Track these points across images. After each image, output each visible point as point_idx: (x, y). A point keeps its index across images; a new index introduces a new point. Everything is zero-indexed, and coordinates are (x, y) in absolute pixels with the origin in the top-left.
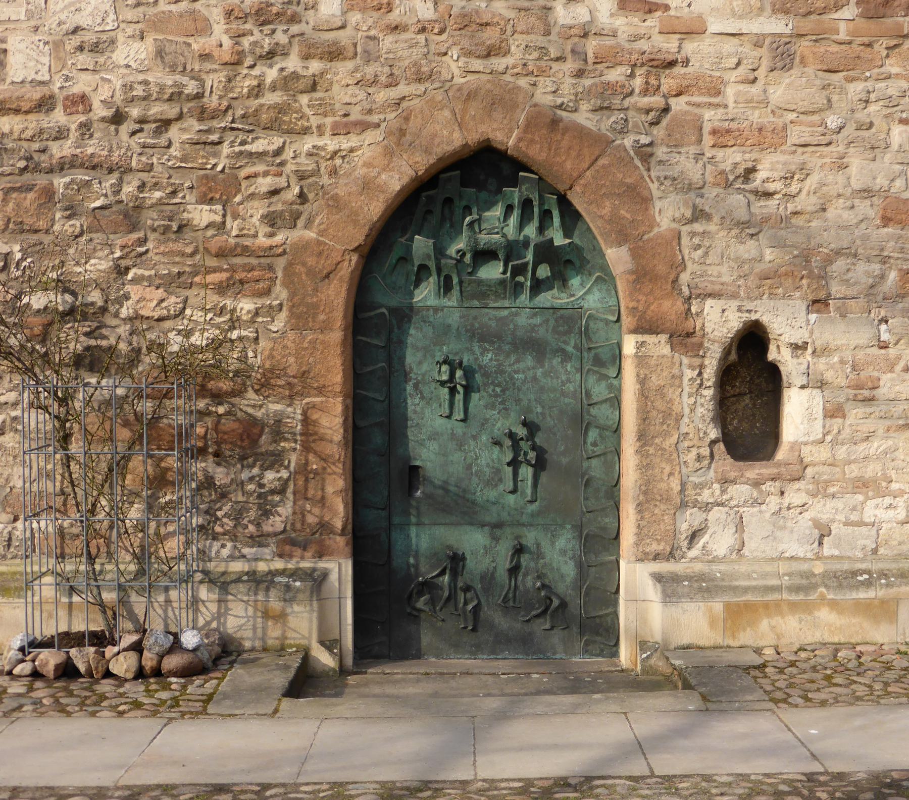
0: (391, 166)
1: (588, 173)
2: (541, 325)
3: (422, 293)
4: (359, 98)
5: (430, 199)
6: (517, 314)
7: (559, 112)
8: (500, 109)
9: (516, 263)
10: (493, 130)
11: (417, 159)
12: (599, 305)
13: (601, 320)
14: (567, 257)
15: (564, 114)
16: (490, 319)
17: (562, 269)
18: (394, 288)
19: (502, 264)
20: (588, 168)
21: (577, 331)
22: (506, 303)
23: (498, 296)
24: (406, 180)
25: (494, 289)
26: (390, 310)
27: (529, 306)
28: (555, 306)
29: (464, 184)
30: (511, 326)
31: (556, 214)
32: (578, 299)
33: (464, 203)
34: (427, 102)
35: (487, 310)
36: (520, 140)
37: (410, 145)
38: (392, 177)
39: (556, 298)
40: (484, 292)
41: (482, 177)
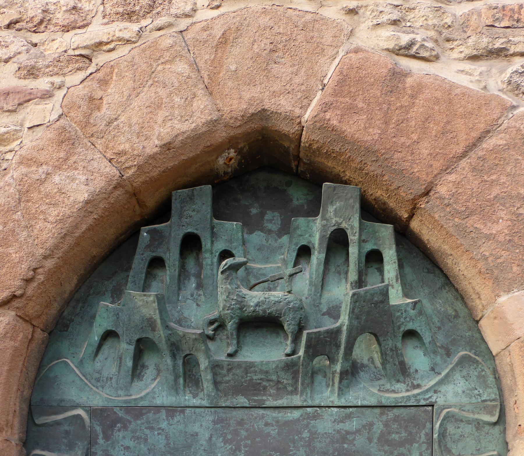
0: (71, 162)
1: (464, 163)
2: (358, 431)
3: (147, 386)
4: (13, 49)
5: (157, 238)
6: (315, 417)
7: (405, 63)
8: (286, 60)
9: (310, 331)
10: (274, 94)
11: (121, 148)
12: (465, 400)
13: (469, 422)
14: (410, 326)
15: (414, 65)
16: (267, 424)
17: (399, 345)
18: (98, 380)
19: (289, 342)
20: (464, 155)
21: (423, 438)
22: (297, 400)
23: (281, 389)
24: (99, 183)
25: (274, 378)
26: (93, 412)
27: (337, 403)
28: (384, 402)
29: (219, 213)
30: (306, 434)
31: (390, 255)
32: (427, 391)
33: (220, 246)
34: (144, 51)
35: (261, 412)
36: (326, 107)
37: (109, 123)
38: (73, 180)
39: (387, 391)
40: (252, 385)
41: (254, 211)
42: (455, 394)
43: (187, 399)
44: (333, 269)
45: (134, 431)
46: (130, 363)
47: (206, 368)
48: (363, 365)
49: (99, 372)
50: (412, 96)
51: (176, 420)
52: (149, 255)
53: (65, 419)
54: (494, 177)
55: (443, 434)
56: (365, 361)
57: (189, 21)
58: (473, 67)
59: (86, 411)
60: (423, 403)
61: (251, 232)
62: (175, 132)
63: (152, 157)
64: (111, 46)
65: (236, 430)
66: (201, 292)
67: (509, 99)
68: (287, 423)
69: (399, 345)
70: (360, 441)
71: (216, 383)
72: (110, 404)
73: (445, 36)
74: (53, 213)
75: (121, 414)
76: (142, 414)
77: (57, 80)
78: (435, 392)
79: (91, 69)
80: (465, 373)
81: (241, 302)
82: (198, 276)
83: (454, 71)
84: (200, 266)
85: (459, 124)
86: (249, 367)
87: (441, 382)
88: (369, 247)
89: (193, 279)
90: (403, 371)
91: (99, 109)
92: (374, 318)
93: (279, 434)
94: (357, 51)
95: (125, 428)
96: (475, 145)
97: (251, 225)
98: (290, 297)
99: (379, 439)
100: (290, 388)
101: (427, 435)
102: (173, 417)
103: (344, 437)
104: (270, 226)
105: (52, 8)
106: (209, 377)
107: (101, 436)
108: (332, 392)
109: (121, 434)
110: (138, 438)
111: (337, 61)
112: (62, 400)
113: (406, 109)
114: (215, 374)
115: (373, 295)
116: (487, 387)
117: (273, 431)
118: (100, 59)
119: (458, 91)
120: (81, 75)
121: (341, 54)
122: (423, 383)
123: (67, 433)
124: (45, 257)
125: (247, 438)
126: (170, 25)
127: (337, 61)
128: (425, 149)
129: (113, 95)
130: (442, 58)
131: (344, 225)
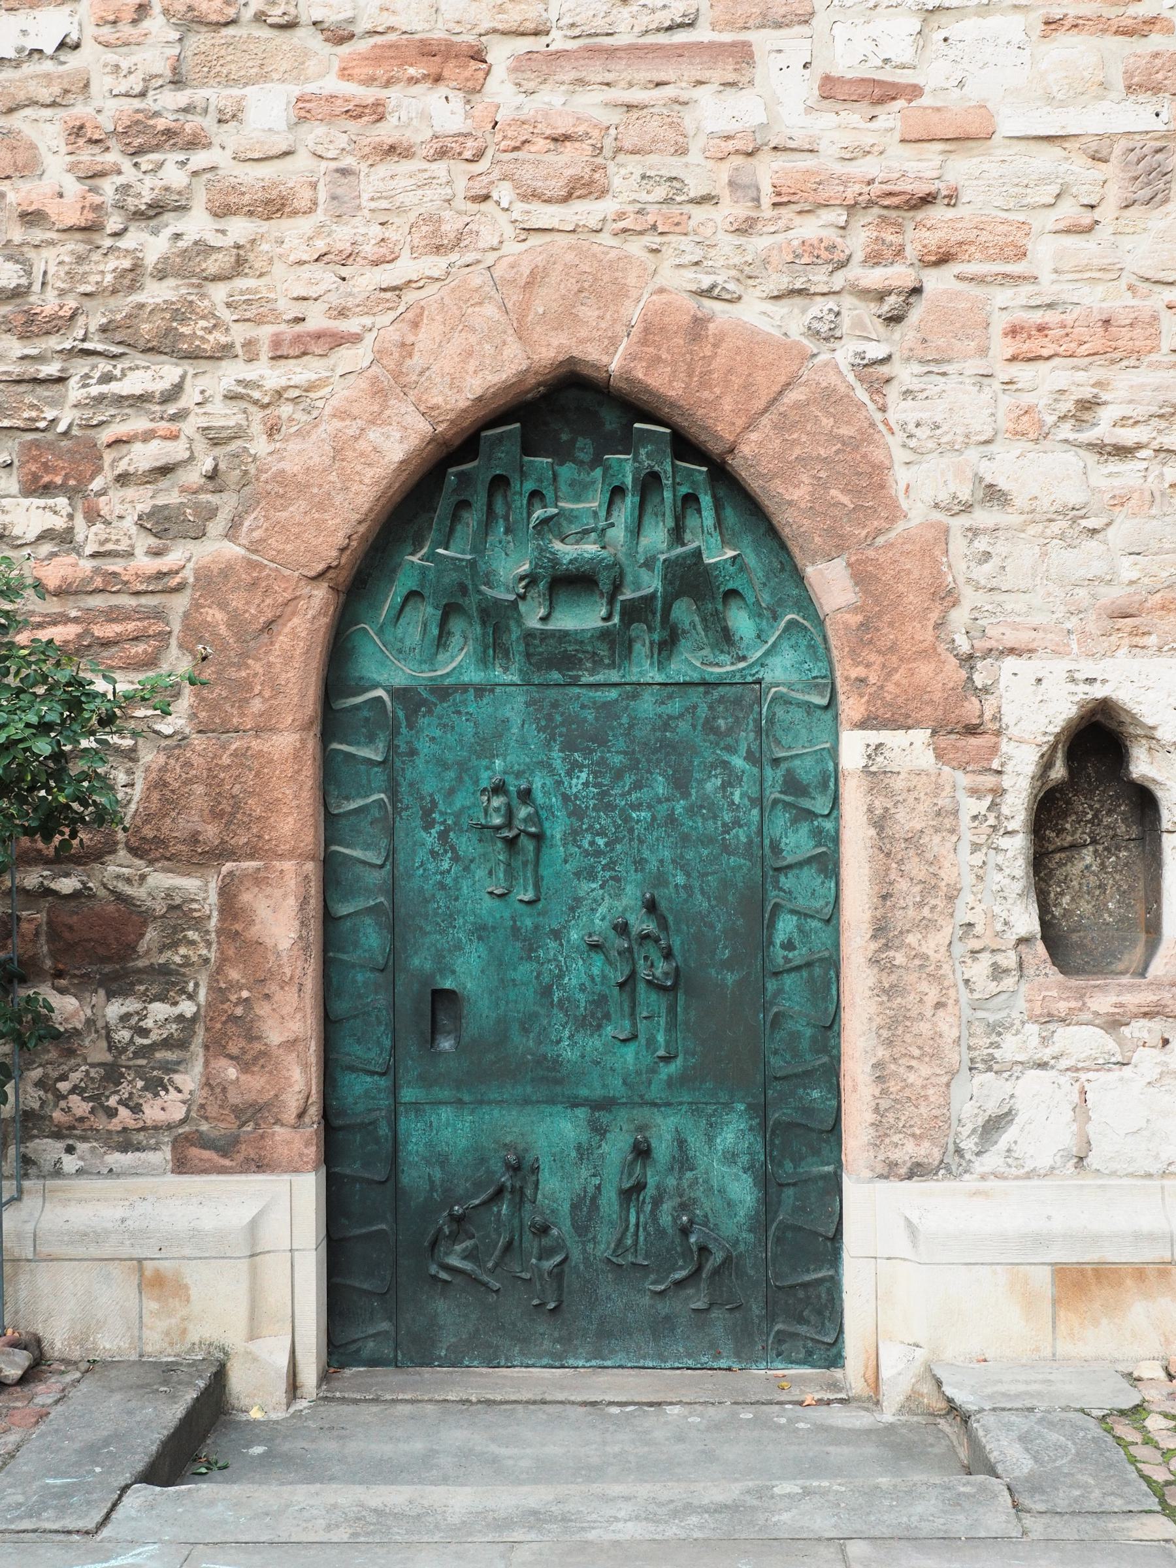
0: (384, 416)
1: (765, 420)
2: (681, 715)
3: (453, 658)
8: (592, 301)
10: (581, 342)
11: (434, 401)
12: (795, 677)
15: (718, 306)
16: (583, 707)
17: (720, 607)
18: (400, 651)
22: (614, 676)
24: (413, 442)
25: (589, 648)
26: (399, 694)
30: (625, 720)
33: (529, 486)
34: (453, 290)
35: (577, 690)
37: (421, 374)
39: (711, 664)
41: (564, 437)
42: (782, 670)
43: (498, 674)
44: (649, 509)
45: (440, 718)
46: (436, 632)
47: (518, 638)
48: (684, 632)
49: (402, 640)
50: (715, 346)
51: (485, 701)
52: (454, 499)
53: (365, 702)
54: (795, 436)
55: (771, 721)
56: (687, 627)
57: (496, 254)
58: (775, 309)
59: (387, 691)
60: (750, 679)
61: (562, 464)
62: (486, 385)
63: (464, 411)
64: (420, 284)
65: (550, 715)
66: (510, 538)
67: (811, 346)
68: (606, 705)
69: (720, 607)
70: (683, 726)
71: (528, 656)
72: (414, 683)
73: (747, 275)
74: (370, 474)
75: (425, 695)
76: (449, 695)
77: (367, 321)
78: (762, 665)
79: (401, 309)
80: (793, 642)
81: (555, 561)
82: (506, 518)
83: (755, 313)
84: (508, 507)
85: (760, 378)
86: (563, 635)
87: (767, 653)
88: (684, 490)
89: (501, 521)
90: (726, 638)
91: (410, 356)
92: (691, 578)
93: (597, 719)
94: (661, 291)
95: (430, 712)
96: (775, 399)
97: (563, 454)
98: (604, 553)
99: (704, 725)
100: (607, 661)
101: (755, 720)
102: (481, 697)
103: (666, 723)
104: (581, 456)
105: (360, 239)
106: (522, 648)
107: (404, 724)
108: (652, 664)
109: (426, 720)
110: (445, 726)
111: (641, 304)
112: (361, 678)
113: (708, 360)
114: (527, 645)
115: (684, 559)
116: (817, 659)
117: (590, 715)
118: (410, 296)
119: (759, 338)
120: (392, 315)
121: (646, 296)
122: (749, 654)
123: (367, 720)
124: (360, 523)
125: (562, 724)
126: (478, 262)
127: (641, 304)
128: (727, 405)
129: (425, 338)
130: (745, 298)
131: (656, 468)
